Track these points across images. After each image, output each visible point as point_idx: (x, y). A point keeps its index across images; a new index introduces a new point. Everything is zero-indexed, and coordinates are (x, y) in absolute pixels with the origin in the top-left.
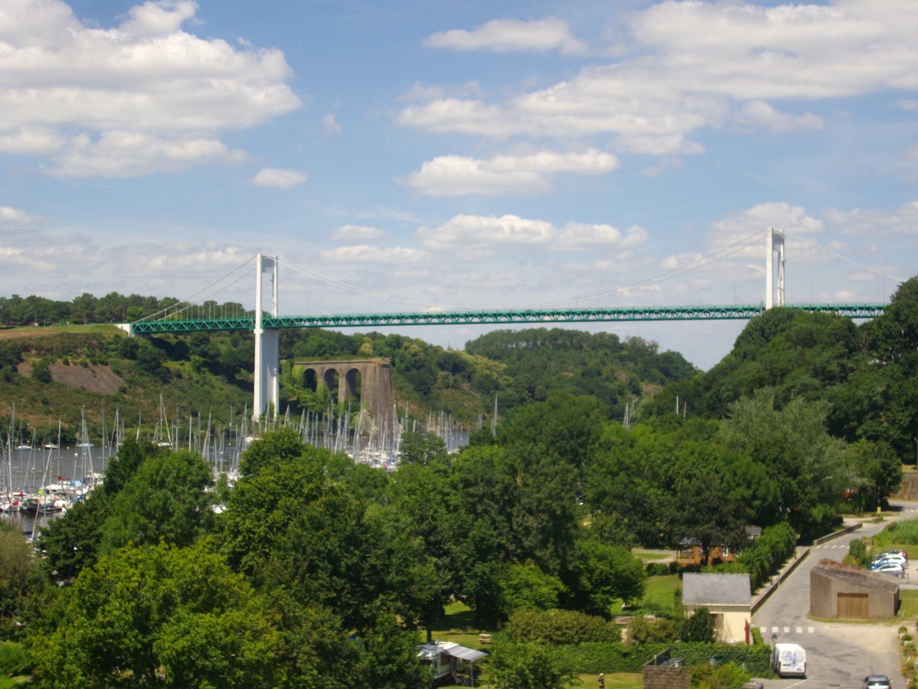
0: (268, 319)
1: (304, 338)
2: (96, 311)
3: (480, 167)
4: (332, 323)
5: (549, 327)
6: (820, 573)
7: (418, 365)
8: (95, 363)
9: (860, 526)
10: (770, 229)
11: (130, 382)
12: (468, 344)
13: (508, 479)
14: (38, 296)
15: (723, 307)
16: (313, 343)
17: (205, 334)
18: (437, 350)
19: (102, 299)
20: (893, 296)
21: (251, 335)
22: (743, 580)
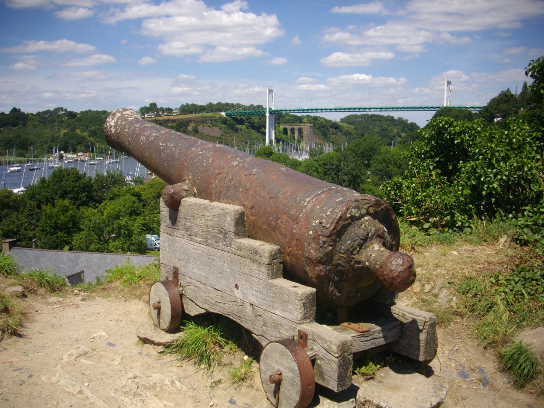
1: (283, 117)
2: (214, 108)
3: (350, 57)
4: (293, 112)
7: (323, 126)
8: (213, 126)
10: (446, 79)
11: (225, 132)
12: (341, 119)
13: (337, 163)
14: (194, 103)
15: (417, 107)
16: (287, 118)
17: (250, 116)
18: (330, 121)
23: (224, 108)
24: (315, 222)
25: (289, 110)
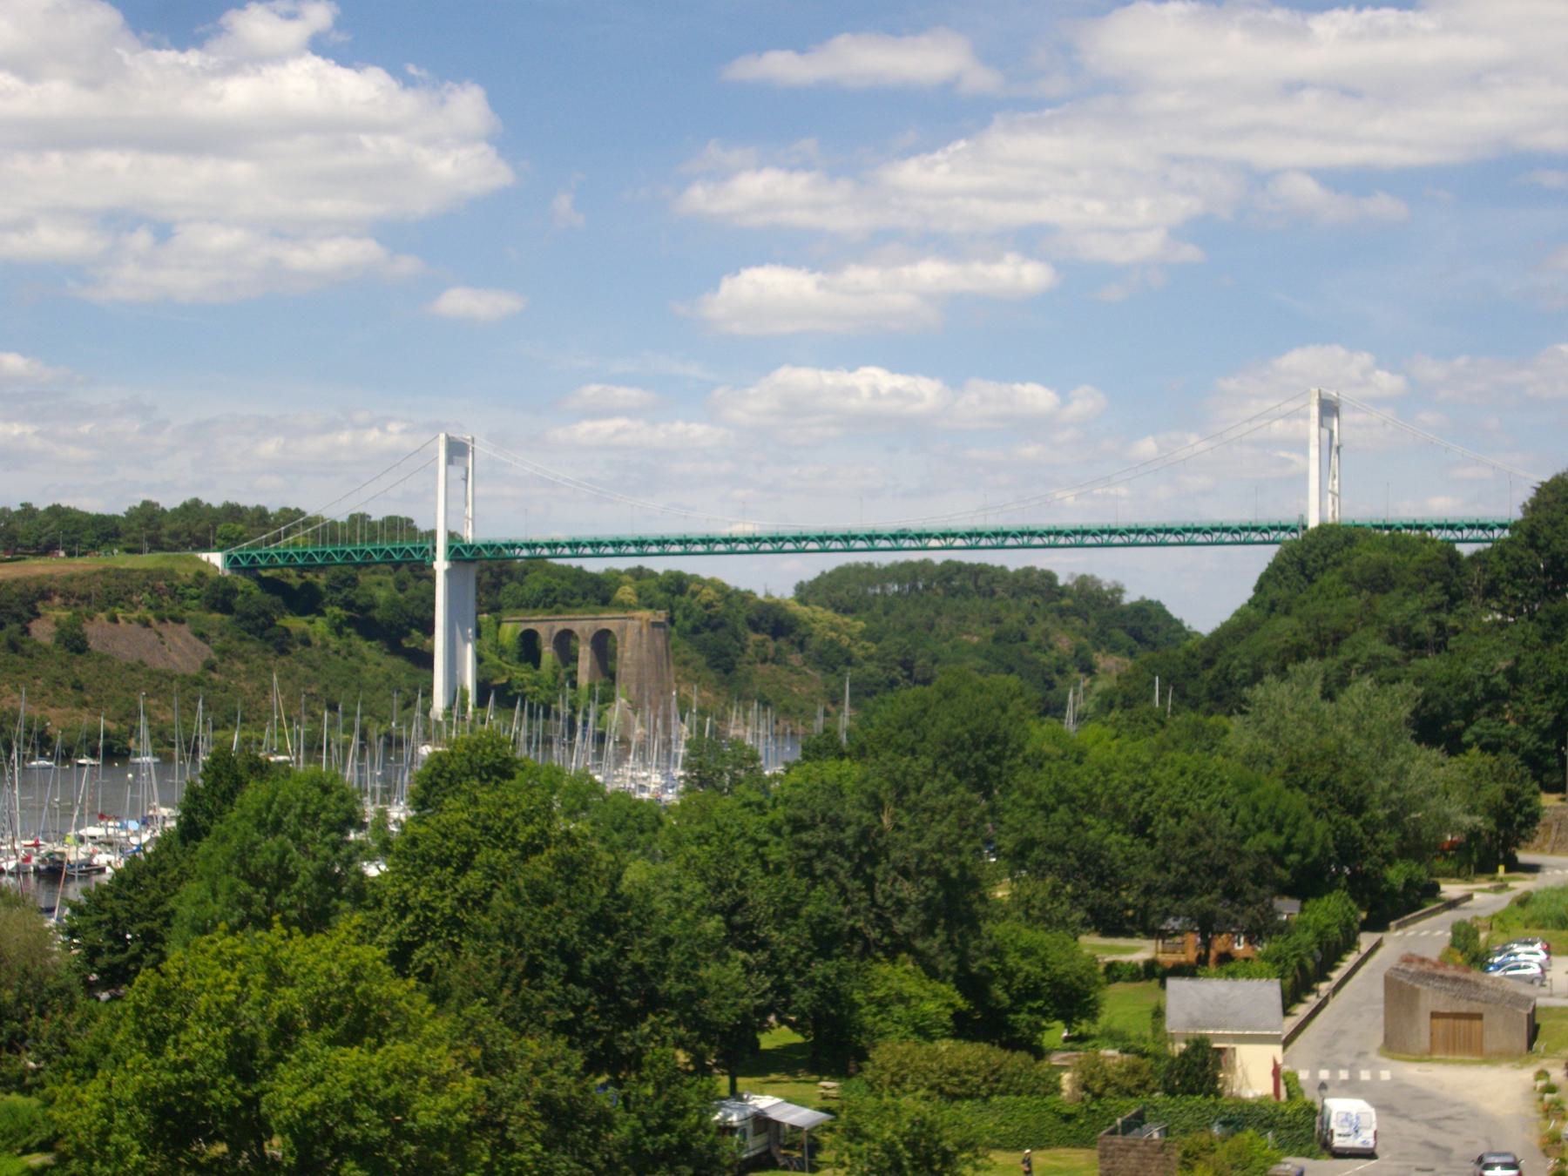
0: (458, 545)
1: (519, 576)
2: (164, 531)
3: (820, 285)
4: (567, 551)
5: (938, 558)
6: (1400, 979)
7: (713, 623)
8: (162, 620)
9: (1469, 897)
10: (1315, 390)
11: (223, 652)
12: (800, 588)
13: (867, 817)
14: (64, 505)
15: (1235, 524)
16: (534, 585)
17: (351, 570)
18: (746, 597)
19: (175, 510)
20: (1525, 505)
21: (428, 572)
22: (1269, 991)
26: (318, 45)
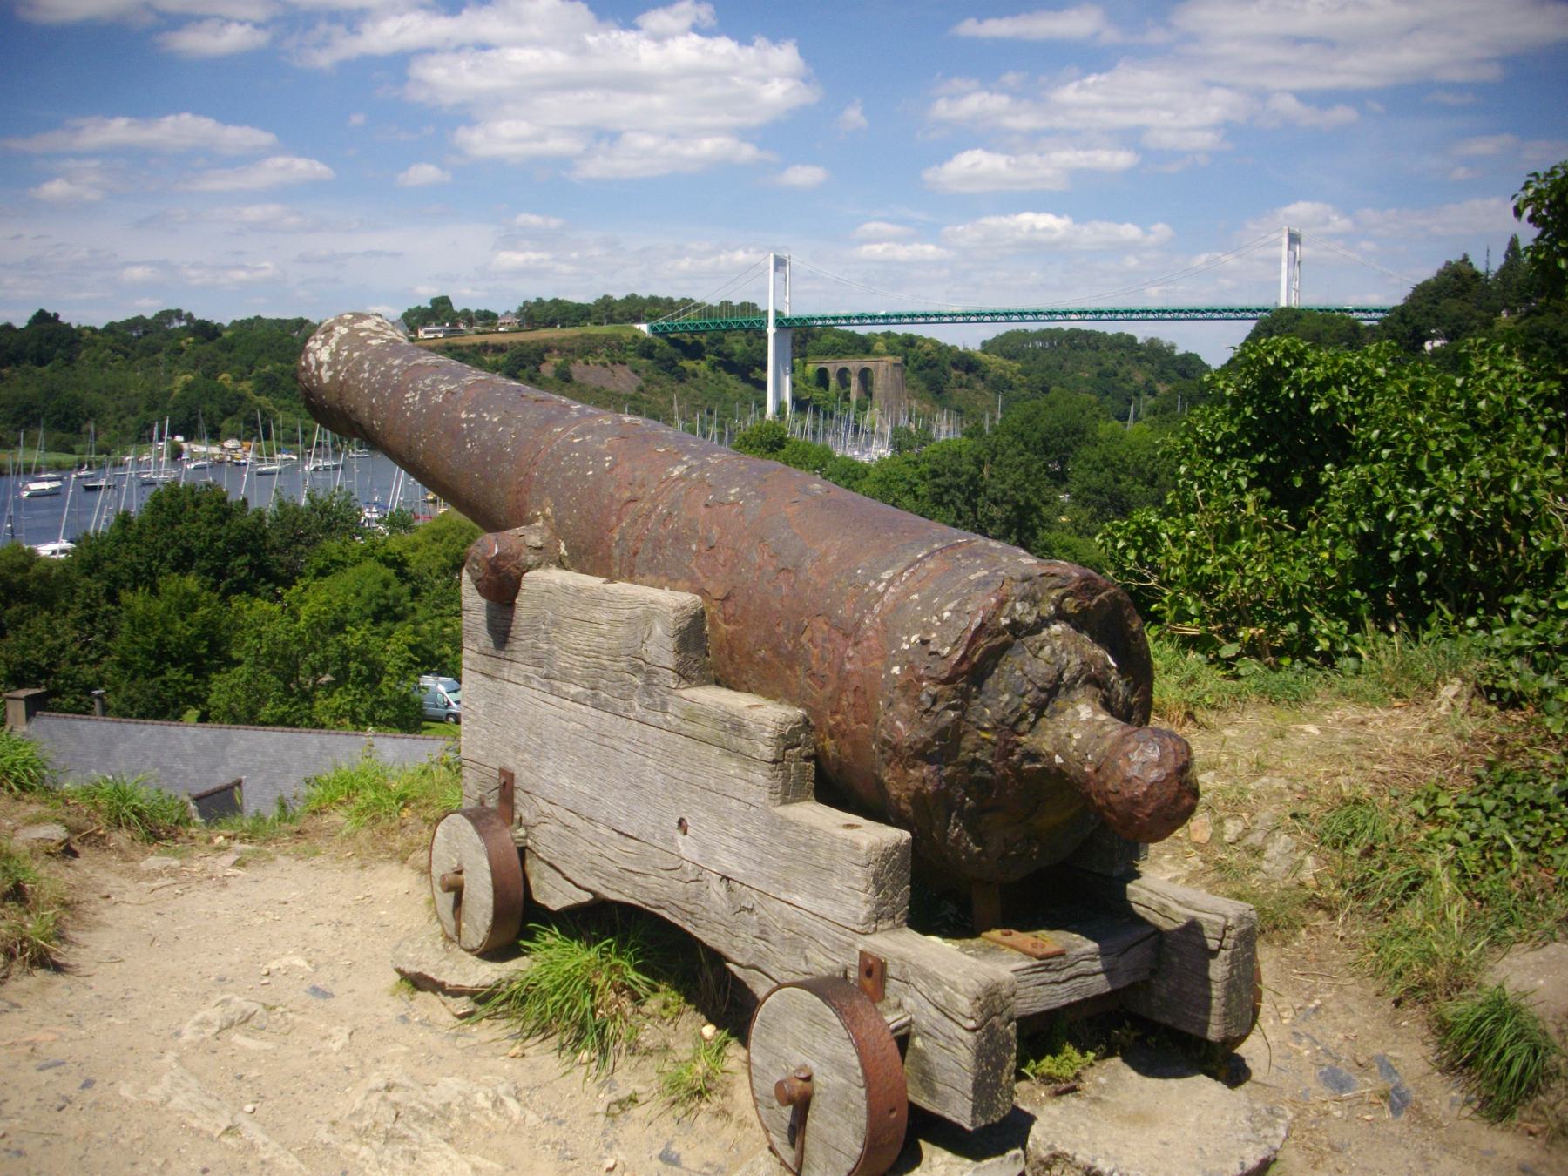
1: (817, 337)
2: (616, 312)
3: (1009, 164)
4: (844, 322)
7: (930, 364)
8: (614, 363)
10: (1286, 228)
11: (647, 381)
12: (984, 344)
13: (972, 469)
14: (560, 298)
15: (1203, 308)
16: (828, 340)
17: (720, 334)
18: (950, 350)
23: (647, 310)
24: (908, 641)
25: (833, 318)
26: (696, 29)
